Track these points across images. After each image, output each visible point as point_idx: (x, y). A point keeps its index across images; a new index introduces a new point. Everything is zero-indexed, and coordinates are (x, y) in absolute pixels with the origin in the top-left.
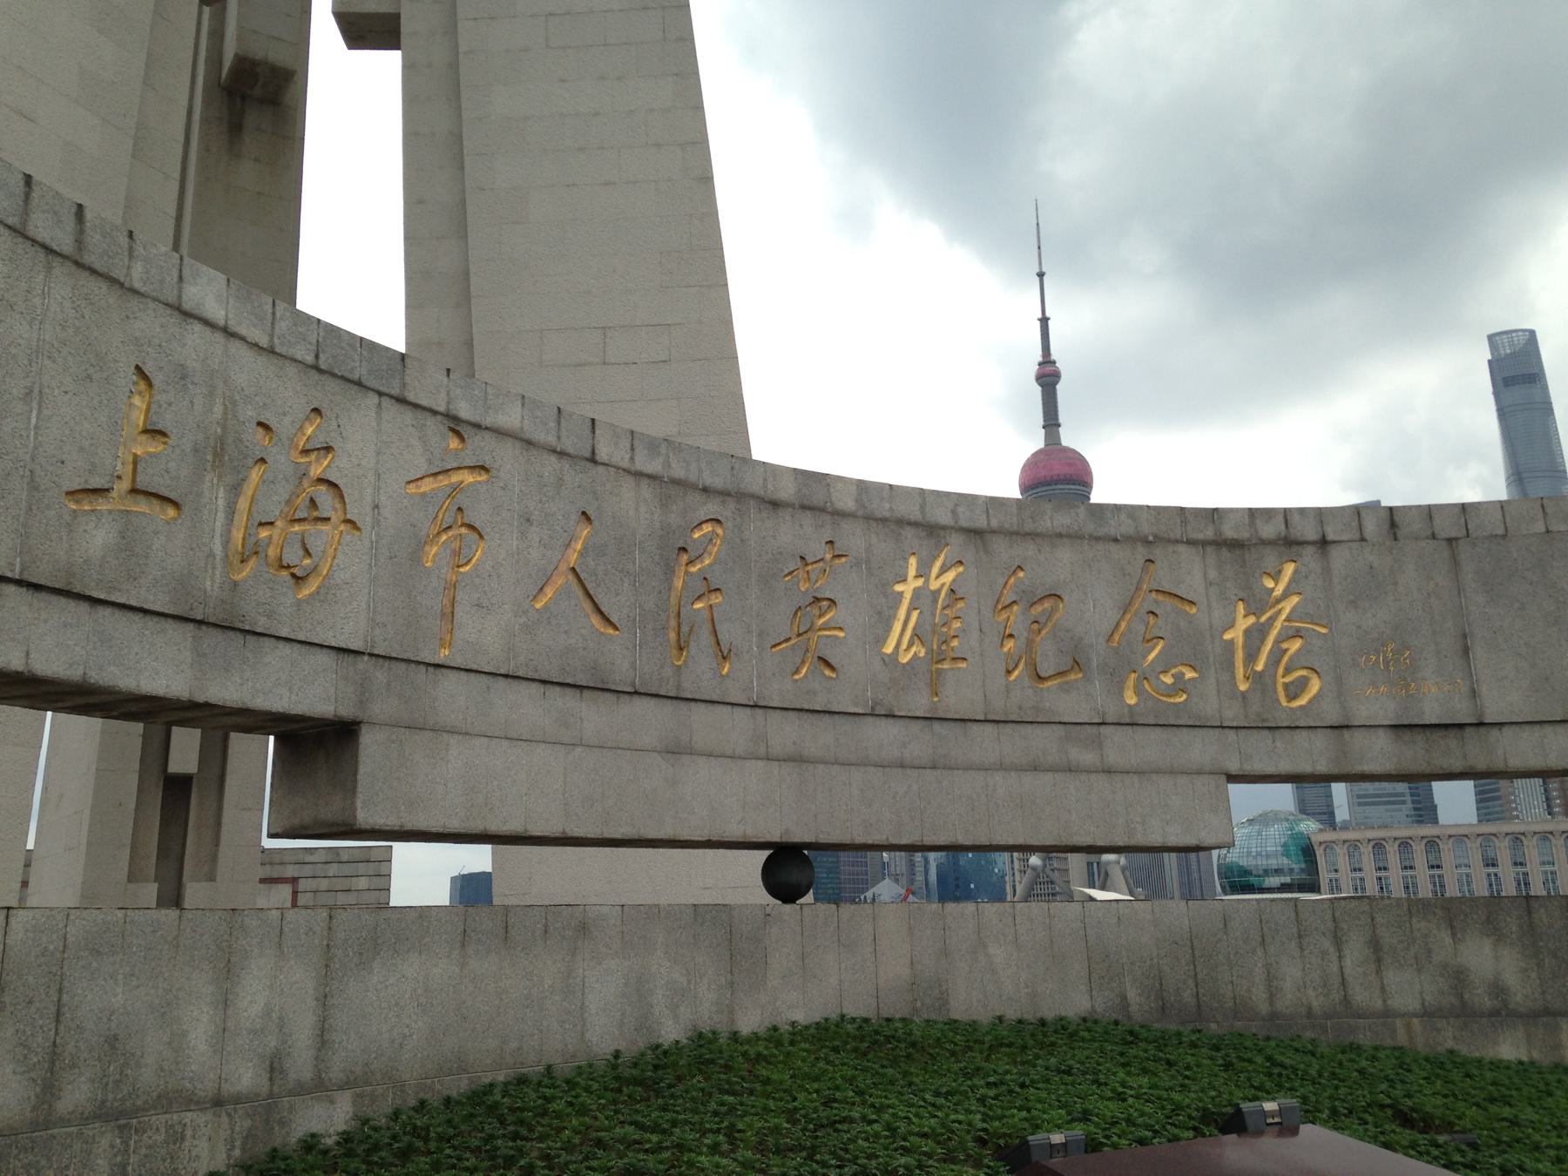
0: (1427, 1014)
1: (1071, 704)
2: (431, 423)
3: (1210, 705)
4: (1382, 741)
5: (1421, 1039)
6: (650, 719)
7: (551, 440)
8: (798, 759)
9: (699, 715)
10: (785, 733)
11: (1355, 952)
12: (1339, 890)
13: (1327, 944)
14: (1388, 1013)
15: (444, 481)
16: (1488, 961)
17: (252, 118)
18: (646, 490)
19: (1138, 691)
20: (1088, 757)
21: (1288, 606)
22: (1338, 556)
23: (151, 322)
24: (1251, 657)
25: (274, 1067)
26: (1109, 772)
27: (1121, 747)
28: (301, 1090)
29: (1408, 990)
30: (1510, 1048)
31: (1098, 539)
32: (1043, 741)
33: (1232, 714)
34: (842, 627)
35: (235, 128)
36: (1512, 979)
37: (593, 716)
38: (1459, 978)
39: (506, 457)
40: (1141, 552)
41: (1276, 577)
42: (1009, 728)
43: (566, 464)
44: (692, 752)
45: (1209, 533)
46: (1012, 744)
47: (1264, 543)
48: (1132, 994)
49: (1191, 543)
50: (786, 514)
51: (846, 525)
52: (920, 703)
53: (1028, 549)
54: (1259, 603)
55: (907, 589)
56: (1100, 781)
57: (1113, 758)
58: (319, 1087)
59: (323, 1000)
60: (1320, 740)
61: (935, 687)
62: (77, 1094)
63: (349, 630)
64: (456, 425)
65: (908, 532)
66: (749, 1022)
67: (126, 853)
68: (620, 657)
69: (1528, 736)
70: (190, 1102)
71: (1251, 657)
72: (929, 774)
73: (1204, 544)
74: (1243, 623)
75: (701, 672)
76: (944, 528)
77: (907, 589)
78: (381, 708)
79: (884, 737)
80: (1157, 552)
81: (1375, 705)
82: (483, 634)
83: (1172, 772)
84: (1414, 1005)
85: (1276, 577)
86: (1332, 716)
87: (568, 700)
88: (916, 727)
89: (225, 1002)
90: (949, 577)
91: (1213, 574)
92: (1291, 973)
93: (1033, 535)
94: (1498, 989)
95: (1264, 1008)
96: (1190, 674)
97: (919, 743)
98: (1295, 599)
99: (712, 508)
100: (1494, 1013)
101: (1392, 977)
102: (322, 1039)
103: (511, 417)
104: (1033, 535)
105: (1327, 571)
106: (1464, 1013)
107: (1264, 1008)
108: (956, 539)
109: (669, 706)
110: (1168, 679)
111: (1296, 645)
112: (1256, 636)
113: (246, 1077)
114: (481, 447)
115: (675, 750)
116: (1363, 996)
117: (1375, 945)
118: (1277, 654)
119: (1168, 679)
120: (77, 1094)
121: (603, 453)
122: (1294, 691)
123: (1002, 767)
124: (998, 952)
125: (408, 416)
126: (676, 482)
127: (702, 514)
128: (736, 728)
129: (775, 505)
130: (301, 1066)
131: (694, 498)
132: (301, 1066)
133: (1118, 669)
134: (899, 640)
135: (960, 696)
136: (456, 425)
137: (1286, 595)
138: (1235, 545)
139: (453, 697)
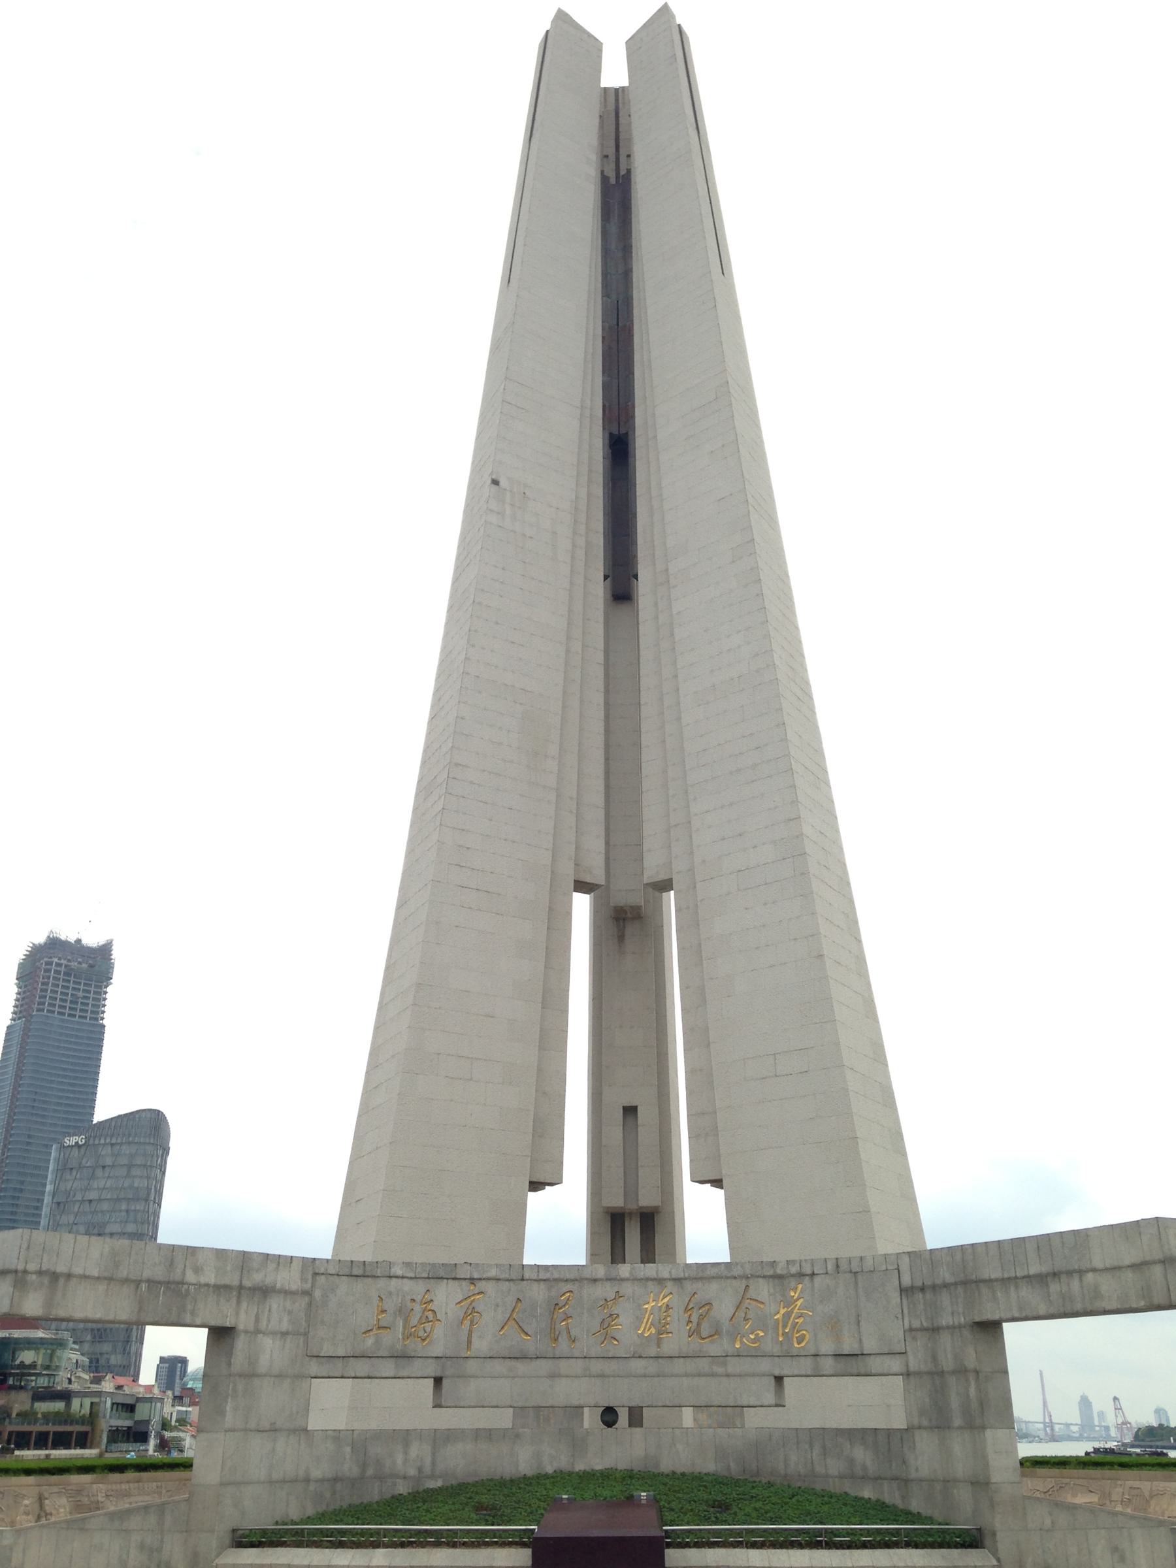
0: (841, 1477)
1: (714, 1349)
2: (464, 1283)
3: (769, 1347)
5: (835, 1486)
6: (544, 1366)
7: (507, 1276)
8: (602, 1376)
9: (563, 1364)
10: (597, 1366)
11: (817, 1450)
13: (807, 1446)
14: (827, 1476)
15: (469, 1300)
16: (862, 1455)
17: (629, 931)
18: (542, 1285)
19: (742, 1342)
20: (719, 1370)
21: (799, 1303)
22: (817, 1280)
23: (382, 1283)
25: (420, 1470)
26: (728, 1375)
27: (734, 1366)
28: (428, 1477)
29: (834, 1466)
30: (867, 1493)
31: (727, 1278)
32: (703, 1365)
33: (776, 1350)
34: (624, 1321)
35: (621, 938)
36: (869, 1463)
37: (521, 1367)
38: (851, 1462)
39: (490, 1287)
40: (744, 1283)
42: (689, 1360)
43: (512, 1284)
44: (560, 1376)
45: (771, 1272)
46: (690, 1366)
47: (792, 1276)
48: (732, 1465)
49: (764, 1277)
50: (599, 1284)
51: (625, 1284)
52: (653, 1351)
53: (699, 1285)
54: (789, 1303)
56: (724, 1379)
57: (730, 1370)
58: (433, 1477)
59: (433, 1454)
60: (809, 1361)
61: (659, 1342)
62: (370, 1472)
63: (438, 1350)
64: (472, 1280)
65: (650, 1283)
66: (580, 1467)
68: (530, 1345)
69: (879, 1359)
70: (398, 1477)
71: (785, 1326)
72: (656, 1379)
73: (771, 1277)
74: (783, 1311)
75: (563, 1346)
76: (665, 1279)
78: (449, 1372)
79: (638, 1366)
80: (751, 1282)
81: (827, 1347)
82: (481, 1345)
83: (753, 1375)
84: (836, 1473)
86: (812, 1352)
87: (513, 1363)
88: (651, 1361)
89: (406, 1453)
90: (665, 1300)
91: (772, 1291)
92: (793, 1458)
93: (701, 1278)
94: (864, 1467)
95: (783, 1472)
96: (762, 1334)
97: (652, 1367)
98: (801, 1300)
99: (569, 1287)
100: (863, 1478)
101: (829, 1461)
102: (433, 1464)
103: (493, 1273)
104: (701, 1278)
105: (813, 1286)
106: (852, 1477)
107: (783, 1472)
108: (669, 1284)
109: (550, 1361)
110: (752, 1337)
111: (801, 1320)
112: (787, 1316)
113: (412, 1472)
114: (482, 1285)
115: (553, 1376)
116: (819, 1469)
117: (824, 1447)
118: (794, 1327)
119: (752, 1337)
120: (370, 1472)
121: (527, 1276)
123: (686, 1375)
124: (680, 1447)
125: (456, 1283)
126: (555, 1280)
127: (565, 1290)
128: (577, 1366)
129: (595, 1280)
130: (427, 1469)
131: (561, 1284)
132: (427, 1469)
133: (734, 1335)
135: (670, 1345)
136: (472, 1280)
137: (798, 1299)
138: (780, 1277)
139: (472, 1366)
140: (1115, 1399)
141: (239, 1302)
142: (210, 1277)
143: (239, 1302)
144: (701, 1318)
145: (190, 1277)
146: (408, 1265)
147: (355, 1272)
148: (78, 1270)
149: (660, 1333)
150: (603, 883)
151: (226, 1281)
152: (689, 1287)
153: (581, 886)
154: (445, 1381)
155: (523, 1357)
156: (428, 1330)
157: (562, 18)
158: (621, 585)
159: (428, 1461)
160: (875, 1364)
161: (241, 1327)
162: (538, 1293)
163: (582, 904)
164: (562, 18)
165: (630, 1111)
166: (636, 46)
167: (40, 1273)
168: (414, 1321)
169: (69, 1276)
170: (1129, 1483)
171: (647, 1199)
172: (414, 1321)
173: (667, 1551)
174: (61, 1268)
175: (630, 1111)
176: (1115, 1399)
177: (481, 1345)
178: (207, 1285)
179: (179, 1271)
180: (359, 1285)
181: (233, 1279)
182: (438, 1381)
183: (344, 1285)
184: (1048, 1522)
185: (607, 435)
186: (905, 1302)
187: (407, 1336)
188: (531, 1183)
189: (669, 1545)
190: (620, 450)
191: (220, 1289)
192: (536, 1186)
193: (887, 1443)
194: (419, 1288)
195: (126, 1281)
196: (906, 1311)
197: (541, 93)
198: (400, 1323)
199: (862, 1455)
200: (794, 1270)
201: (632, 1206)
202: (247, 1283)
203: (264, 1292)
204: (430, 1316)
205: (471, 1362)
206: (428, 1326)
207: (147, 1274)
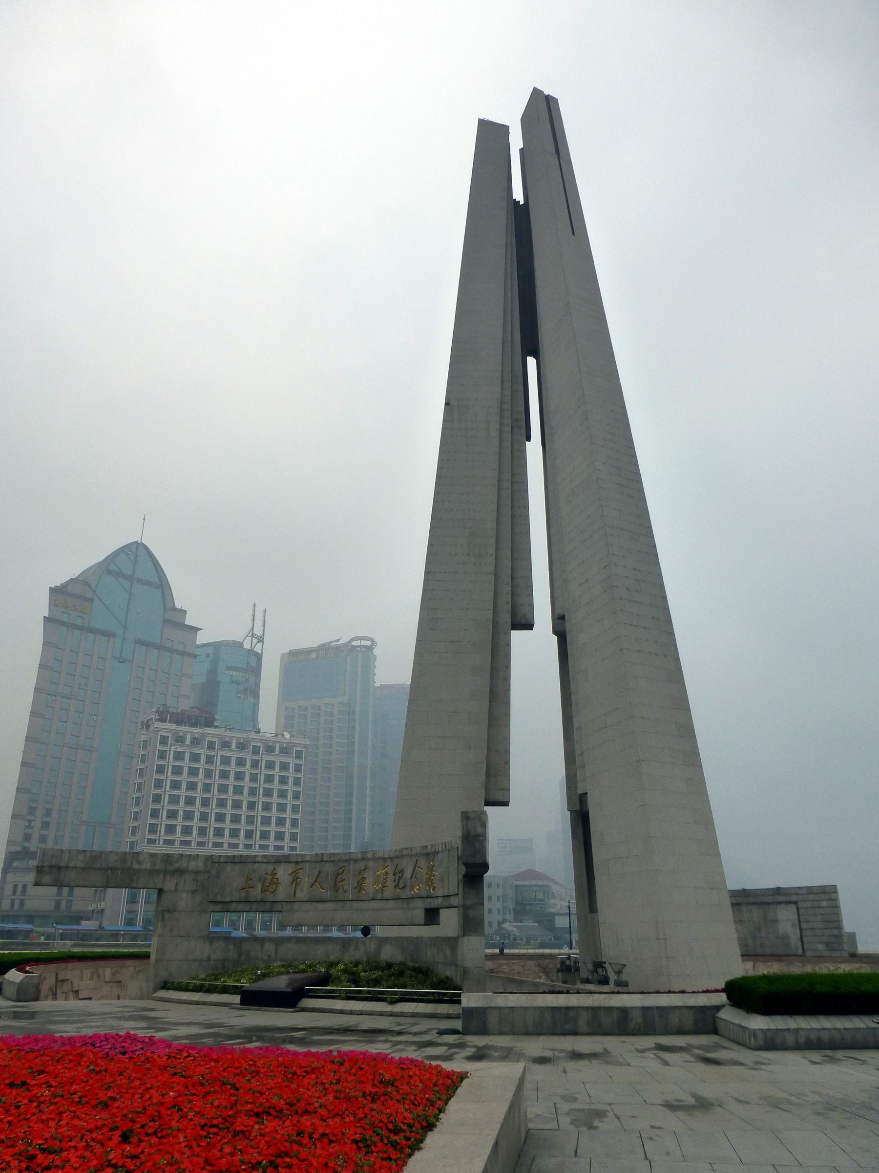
25: (269, 956)
37: (320, 906)
39: (307, 866)
52: (379, 896)
58: (276, 960)
68: (327, 894)
75: (341, 895)
79: (373, 904)
103: (308, 858)
114: (301, 865)
136: (297, 863)
141: (164, 877)
142: (147, 865)
143: (164, 877)
144: (400, 878)
145: (136, 866)
147: (236, 861)
148: (72, 864)
149: (383, 887)
151: (157, 868)
152: (396, 862)
155: (322, 901)
157: (535, 89)
159: (273, 952)
162: (329, 868)
164: (535, 89)
166: (526, 120)
167: (51, 866)
168: (267, 884)
169: (67, 868)
172: (267, 884)
174: (62, 864)
177: (299, 895)
178: (145, 870)
179: (129, 864)
180: (237, 867)
181: (159, 866)
183: (229, 868)
187: (263, 890)
191: (153, 872)
194: (270, 868)
195: (99, 869)
197: (549, 126)
198: (260, 885)
202: (170, 868)
203: (181, 872)
204: (275, 882)
205: (297, 904)
207: (111, 865)
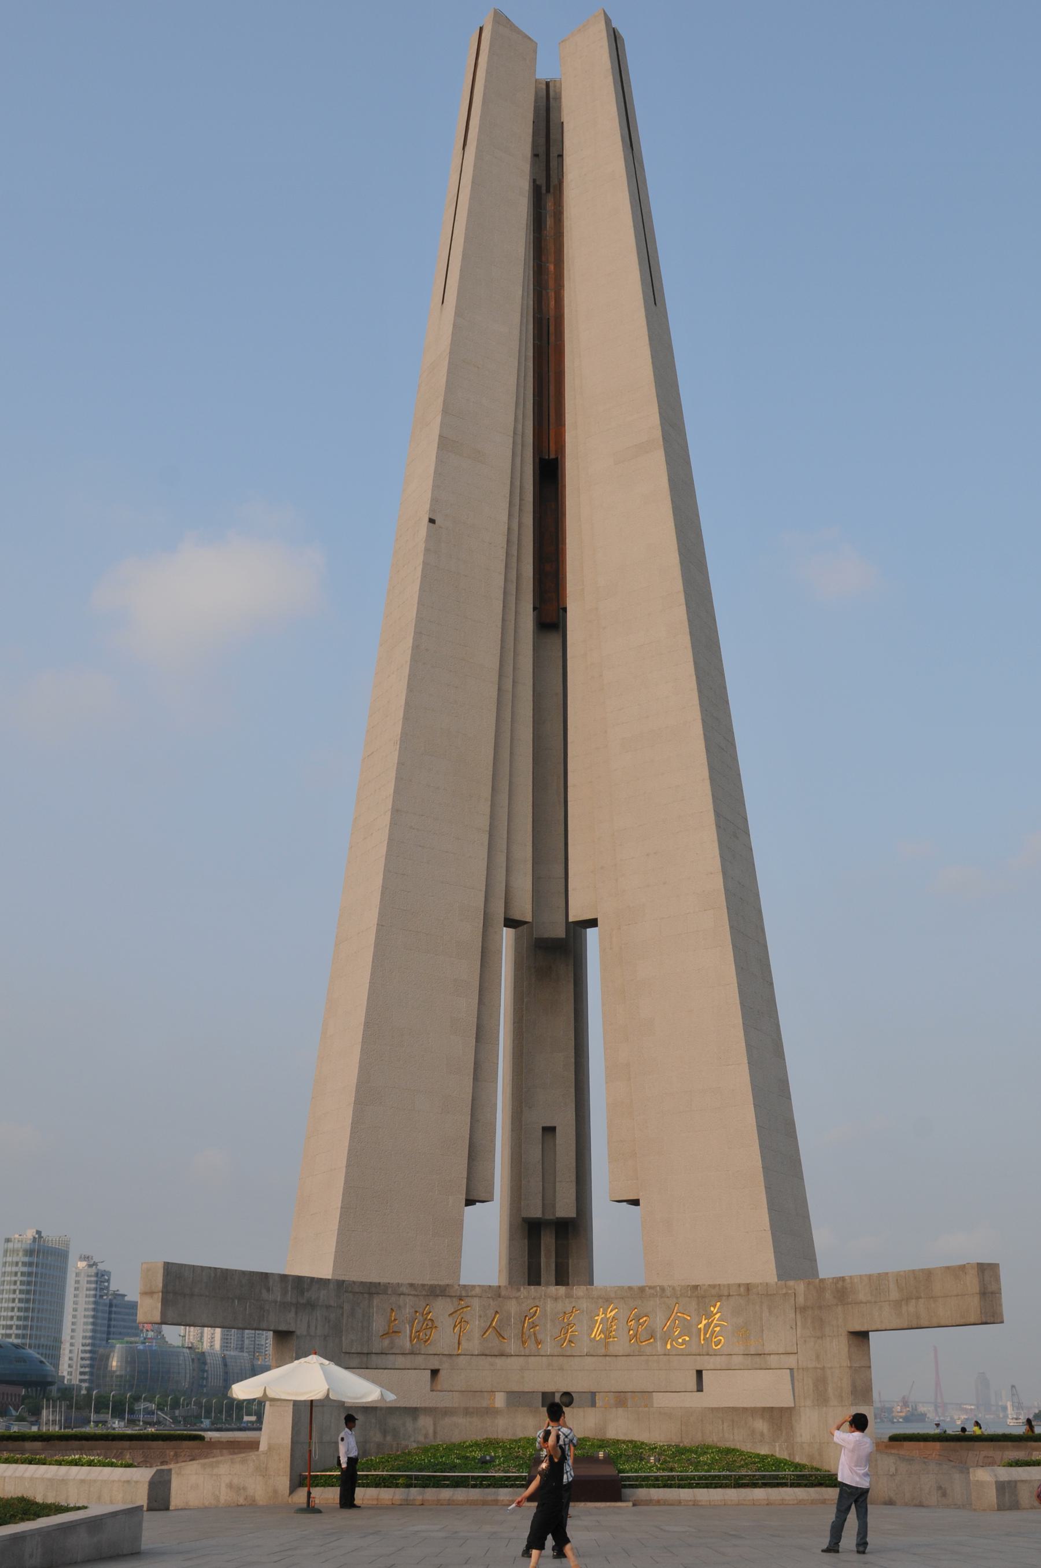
4: (741, 1358)
12: (1002, 1487)
19: (672, 1344)
24: (705, 1334)
36: (765, 1431)
41: (715, 1306)
52: (603, 1351)
54: (709, 1315)
55: (599, 1318)
59: (435, 1424)
61: (607, 1345)
67: (573, 1090)
71: (705, 1334)
74: (704, 1322)
77: (599, 1318)
85: (715, 1306)
88: (601, 1358)
102: (435, 1433)
111: (717, 1329)
122: (717, 1343)
134: (596, 1333)
140: (1013, 1387)
146: (411, 1285)
150: (529, 919)
153: (510, 923)
154: (442, 1373)
156: (428, 1333)
158: (550, 618)
160: (773, 1360)
161: (298, 1333)
163: (507, 936)
165: (549, 1131)
170: (984, 1453)
171: (565, 1209)
173: (623, 1490)
175: (549, 1131)
176: (1013, 1387)
182: (435, 1373)
184: (893, 1470)
185: (537, 460)
186: (798, 1316)
188: (467, 1200)
189: (625, 1486)
190: (549, 474)
192: (469, 1202)
193: (780, 1417)
196: (799, 1324)
199: (761, 1425)
200: (714, 1292)
201: (549, 1216)
205: (462, 1357)
206: (428, 1332)
